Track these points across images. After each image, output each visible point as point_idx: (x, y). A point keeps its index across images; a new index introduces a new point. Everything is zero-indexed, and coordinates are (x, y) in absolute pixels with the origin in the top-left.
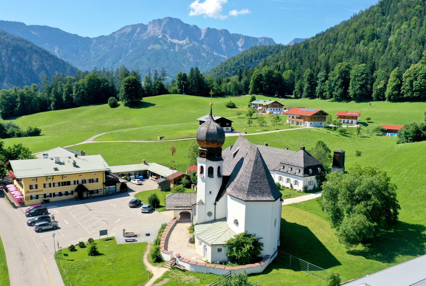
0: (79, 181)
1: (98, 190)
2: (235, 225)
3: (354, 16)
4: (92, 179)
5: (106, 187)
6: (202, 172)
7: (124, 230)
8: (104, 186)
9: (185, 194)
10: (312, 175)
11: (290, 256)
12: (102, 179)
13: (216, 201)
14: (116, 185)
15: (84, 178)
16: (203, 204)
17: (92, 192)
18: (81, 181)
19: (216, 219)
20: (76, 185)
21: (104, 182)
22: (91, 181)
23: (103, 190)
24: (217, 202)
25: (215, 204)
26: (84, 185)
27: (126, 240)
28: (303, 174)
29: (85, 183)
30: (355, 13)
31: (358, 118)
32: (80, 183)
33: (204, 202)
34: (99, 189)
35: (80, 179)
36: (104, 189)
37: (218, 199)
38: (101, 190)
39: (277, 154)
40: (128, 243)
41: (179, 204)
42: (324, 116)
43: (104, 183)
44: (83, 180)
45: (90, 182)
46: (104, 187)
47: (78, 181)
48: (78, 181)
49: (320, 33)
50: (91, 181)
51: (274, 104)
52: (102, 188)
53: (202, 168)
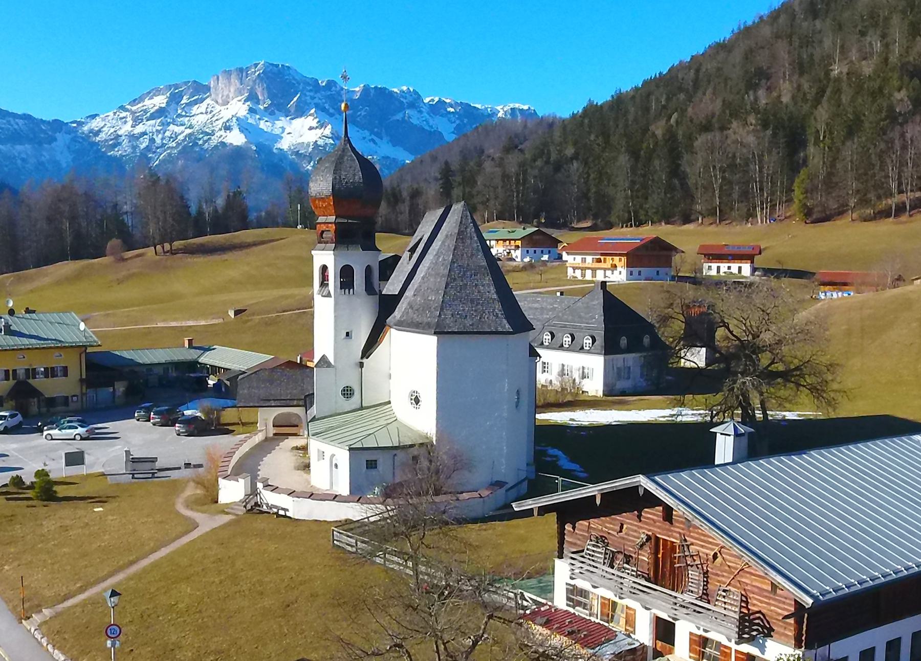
0: (18, 372)
1: (67, 398)
2: (411, 407)
3: (739, 28)
4: (53, 368)
5: (88, 390)
6: (324, 282)
7: (128, 452)
8: (84, 388)
9: (288, 372)
10: (628, 350)
11: (557, 479)
12: (77, 370)
13: (362, 358)
14: (114, 387)
15: (31, 365)
16: (329, 365)
17: (51, 402)
18: (23, 371)
19: (364, 405)
20: (12, 382)
21: (84, 377)
22: (50, 372)
23: (79, 398)
24: (365, 360)
25: (361, 365)
26: (31, 381)
27: (133, 474)
28: (602, 347)
29: (34, 377)
30: (742, 22)
31: (756, 258)
32: (21, 373)
33: (331, 359)
34: (69, 395)
35: (21, 367)
36: (82, 394)
37: (367, 351)
38: (75, 399)
39: (536, 309)
40: (135, 480)
41: (273, 393)
42: (665, 253)
43: (81, 380)
44: (27, 370)
45: (46, 376)
46: (84, 391)
47: (14, 371)
48: (16, 370)
49: (653, 76)
50: (50, 372)
51: (535, 237)
52: (78, 392)
53: (324, 268)
